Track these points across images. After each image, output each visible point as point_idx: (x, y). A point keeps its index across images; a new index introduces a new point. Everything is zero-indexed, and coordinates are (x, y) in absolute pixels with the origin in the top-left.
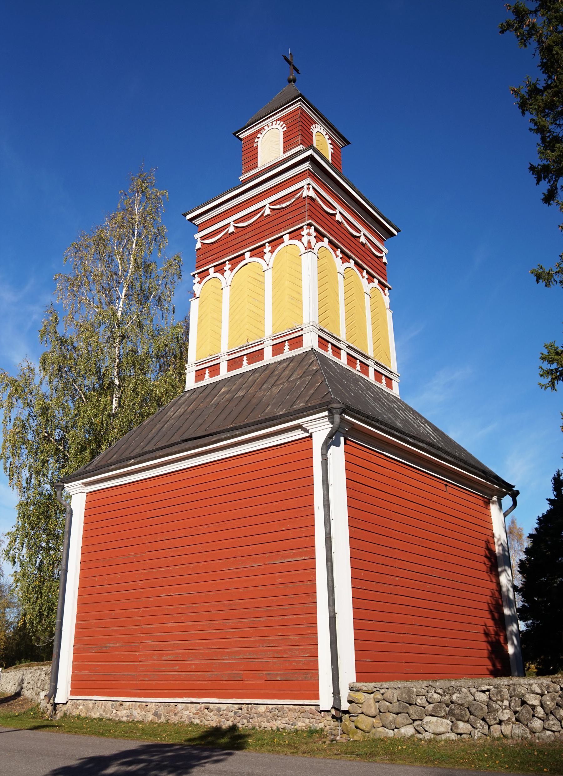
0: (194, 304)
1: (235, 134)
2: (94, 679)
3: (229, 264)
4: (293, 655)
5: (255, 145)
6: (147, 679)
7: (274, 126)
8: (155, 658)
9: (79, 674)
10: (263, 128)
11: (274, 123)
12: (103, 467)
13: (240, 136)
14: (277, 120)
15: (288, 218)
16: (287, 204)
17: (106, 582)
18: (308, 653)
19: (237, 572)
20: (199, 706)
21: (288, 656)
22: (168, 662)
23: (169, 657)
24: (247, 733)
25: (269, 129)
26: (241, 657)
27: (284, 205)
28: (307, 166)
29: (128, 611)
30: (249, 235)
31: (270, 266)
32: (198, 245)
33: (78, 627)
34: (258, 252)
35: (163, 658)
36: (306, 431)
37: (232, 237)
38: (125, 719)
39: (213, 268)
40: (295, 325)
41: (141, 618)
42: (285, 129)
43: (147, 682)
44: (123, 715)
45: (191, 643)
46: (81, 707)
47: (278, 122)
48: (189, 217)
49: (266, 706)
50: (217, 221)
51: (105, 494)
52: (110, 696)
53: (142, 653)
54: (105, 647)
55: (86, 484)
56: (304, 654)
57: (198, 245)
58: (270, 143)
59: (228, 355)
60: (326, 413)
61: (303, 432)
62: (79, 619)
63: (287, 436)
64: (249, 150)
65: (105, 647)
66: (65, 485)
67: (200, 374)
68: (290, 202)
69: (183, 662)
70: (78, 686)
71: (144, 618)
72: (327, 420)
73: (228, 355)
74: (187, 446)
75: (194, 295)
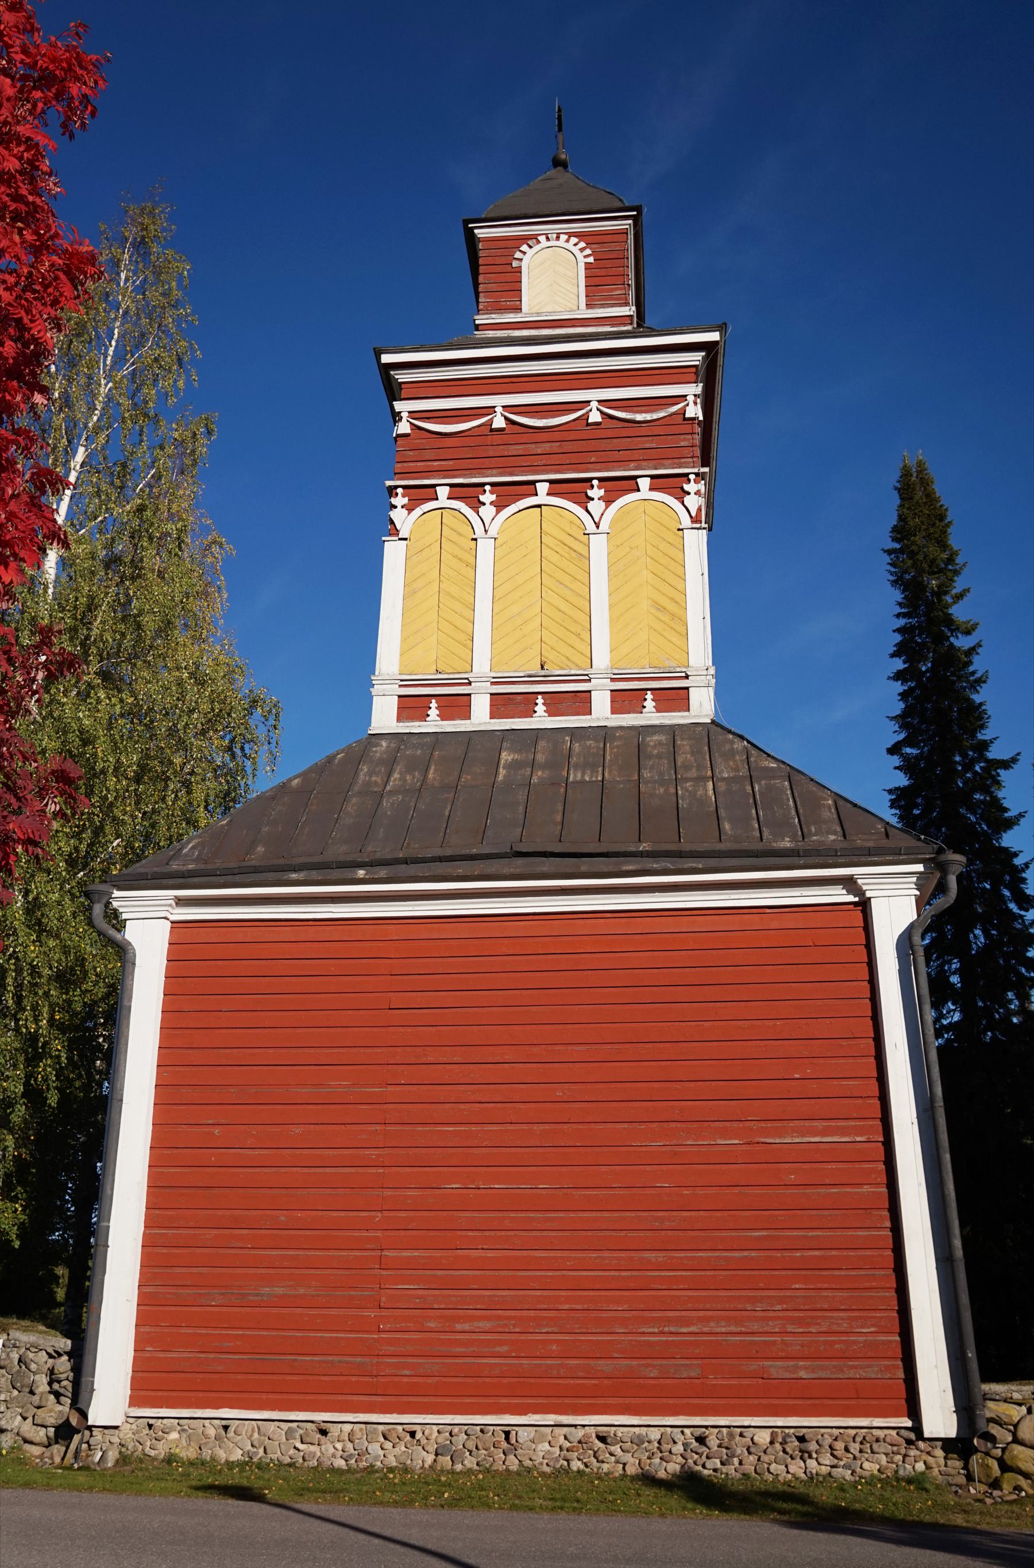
0: (394, 552)
1: (466, 222)
2: (220, 1368)
3: (492, 492)
4: (835, 1328)
5: (515, 264)
6: (407, 1373)
7: (570, 246)
8: (432, 1325)
9: (162, 1355)
10: (535, 237)
11: (564, 237)
12: (256, 870)
13: (476, 231)
14: (570, 235)
15: (647, 446)
16: (648, 417)
17: (250, 1142)
18: (873, 1325)
19: (676, 1153)
20: (580, 1433)
21: (822, 1329)
22: (474, 1337)
23: (476, 1324)
24: (200, 1494)
25: (549, 244)
26: (692, 1329)
27: (639, 417)
28: (696, 358)
29: (335, 1214)
30: (546, 447)
31: (604, 526)
32: (404, 427)
33: (148, 1243)
34: (575, 491)
35: (459, 1327)
36: (859, 892)
37: (498, 439)
38: (340, 1463)
39: (448, 488)
40: (667, 664)
41: (379, 1234)
42: (591, 260)
43: (406, 1380)
44: (331, 1453)
45: (546, 1297)
46: (174, 1435)
47: (574, 240)
48: (386, 358)
49: (535, 1428)
50: (439, 391)
51: (239, 935)
52: (280, 1410)
53: (385, 1313)
54: (257, 1295)
55: (180, 902)
56: (862, 1327)
57: (404, 427)
58: (553, 273)
59: (493, 683)
60: (920, 868)
61: (844, 892)
62: (150, 1223)
63: (793, 894)
64: (498, 269)
65: (257, 1295)
66: (117, 893)
67: (411, 706)
68: (655, 416)
69: (523, 1337)
70: (145, 1387)
71: (389, 1233)
72: (914, 879)
73: (493, 683)
74: (545, 869)
75: (394, 531)
